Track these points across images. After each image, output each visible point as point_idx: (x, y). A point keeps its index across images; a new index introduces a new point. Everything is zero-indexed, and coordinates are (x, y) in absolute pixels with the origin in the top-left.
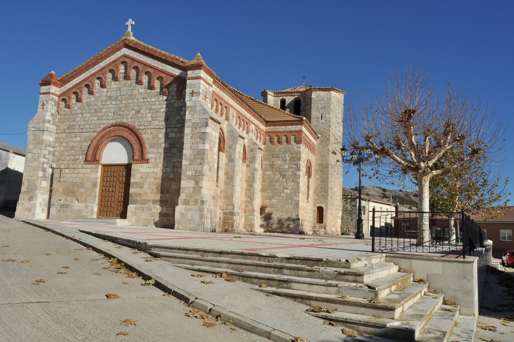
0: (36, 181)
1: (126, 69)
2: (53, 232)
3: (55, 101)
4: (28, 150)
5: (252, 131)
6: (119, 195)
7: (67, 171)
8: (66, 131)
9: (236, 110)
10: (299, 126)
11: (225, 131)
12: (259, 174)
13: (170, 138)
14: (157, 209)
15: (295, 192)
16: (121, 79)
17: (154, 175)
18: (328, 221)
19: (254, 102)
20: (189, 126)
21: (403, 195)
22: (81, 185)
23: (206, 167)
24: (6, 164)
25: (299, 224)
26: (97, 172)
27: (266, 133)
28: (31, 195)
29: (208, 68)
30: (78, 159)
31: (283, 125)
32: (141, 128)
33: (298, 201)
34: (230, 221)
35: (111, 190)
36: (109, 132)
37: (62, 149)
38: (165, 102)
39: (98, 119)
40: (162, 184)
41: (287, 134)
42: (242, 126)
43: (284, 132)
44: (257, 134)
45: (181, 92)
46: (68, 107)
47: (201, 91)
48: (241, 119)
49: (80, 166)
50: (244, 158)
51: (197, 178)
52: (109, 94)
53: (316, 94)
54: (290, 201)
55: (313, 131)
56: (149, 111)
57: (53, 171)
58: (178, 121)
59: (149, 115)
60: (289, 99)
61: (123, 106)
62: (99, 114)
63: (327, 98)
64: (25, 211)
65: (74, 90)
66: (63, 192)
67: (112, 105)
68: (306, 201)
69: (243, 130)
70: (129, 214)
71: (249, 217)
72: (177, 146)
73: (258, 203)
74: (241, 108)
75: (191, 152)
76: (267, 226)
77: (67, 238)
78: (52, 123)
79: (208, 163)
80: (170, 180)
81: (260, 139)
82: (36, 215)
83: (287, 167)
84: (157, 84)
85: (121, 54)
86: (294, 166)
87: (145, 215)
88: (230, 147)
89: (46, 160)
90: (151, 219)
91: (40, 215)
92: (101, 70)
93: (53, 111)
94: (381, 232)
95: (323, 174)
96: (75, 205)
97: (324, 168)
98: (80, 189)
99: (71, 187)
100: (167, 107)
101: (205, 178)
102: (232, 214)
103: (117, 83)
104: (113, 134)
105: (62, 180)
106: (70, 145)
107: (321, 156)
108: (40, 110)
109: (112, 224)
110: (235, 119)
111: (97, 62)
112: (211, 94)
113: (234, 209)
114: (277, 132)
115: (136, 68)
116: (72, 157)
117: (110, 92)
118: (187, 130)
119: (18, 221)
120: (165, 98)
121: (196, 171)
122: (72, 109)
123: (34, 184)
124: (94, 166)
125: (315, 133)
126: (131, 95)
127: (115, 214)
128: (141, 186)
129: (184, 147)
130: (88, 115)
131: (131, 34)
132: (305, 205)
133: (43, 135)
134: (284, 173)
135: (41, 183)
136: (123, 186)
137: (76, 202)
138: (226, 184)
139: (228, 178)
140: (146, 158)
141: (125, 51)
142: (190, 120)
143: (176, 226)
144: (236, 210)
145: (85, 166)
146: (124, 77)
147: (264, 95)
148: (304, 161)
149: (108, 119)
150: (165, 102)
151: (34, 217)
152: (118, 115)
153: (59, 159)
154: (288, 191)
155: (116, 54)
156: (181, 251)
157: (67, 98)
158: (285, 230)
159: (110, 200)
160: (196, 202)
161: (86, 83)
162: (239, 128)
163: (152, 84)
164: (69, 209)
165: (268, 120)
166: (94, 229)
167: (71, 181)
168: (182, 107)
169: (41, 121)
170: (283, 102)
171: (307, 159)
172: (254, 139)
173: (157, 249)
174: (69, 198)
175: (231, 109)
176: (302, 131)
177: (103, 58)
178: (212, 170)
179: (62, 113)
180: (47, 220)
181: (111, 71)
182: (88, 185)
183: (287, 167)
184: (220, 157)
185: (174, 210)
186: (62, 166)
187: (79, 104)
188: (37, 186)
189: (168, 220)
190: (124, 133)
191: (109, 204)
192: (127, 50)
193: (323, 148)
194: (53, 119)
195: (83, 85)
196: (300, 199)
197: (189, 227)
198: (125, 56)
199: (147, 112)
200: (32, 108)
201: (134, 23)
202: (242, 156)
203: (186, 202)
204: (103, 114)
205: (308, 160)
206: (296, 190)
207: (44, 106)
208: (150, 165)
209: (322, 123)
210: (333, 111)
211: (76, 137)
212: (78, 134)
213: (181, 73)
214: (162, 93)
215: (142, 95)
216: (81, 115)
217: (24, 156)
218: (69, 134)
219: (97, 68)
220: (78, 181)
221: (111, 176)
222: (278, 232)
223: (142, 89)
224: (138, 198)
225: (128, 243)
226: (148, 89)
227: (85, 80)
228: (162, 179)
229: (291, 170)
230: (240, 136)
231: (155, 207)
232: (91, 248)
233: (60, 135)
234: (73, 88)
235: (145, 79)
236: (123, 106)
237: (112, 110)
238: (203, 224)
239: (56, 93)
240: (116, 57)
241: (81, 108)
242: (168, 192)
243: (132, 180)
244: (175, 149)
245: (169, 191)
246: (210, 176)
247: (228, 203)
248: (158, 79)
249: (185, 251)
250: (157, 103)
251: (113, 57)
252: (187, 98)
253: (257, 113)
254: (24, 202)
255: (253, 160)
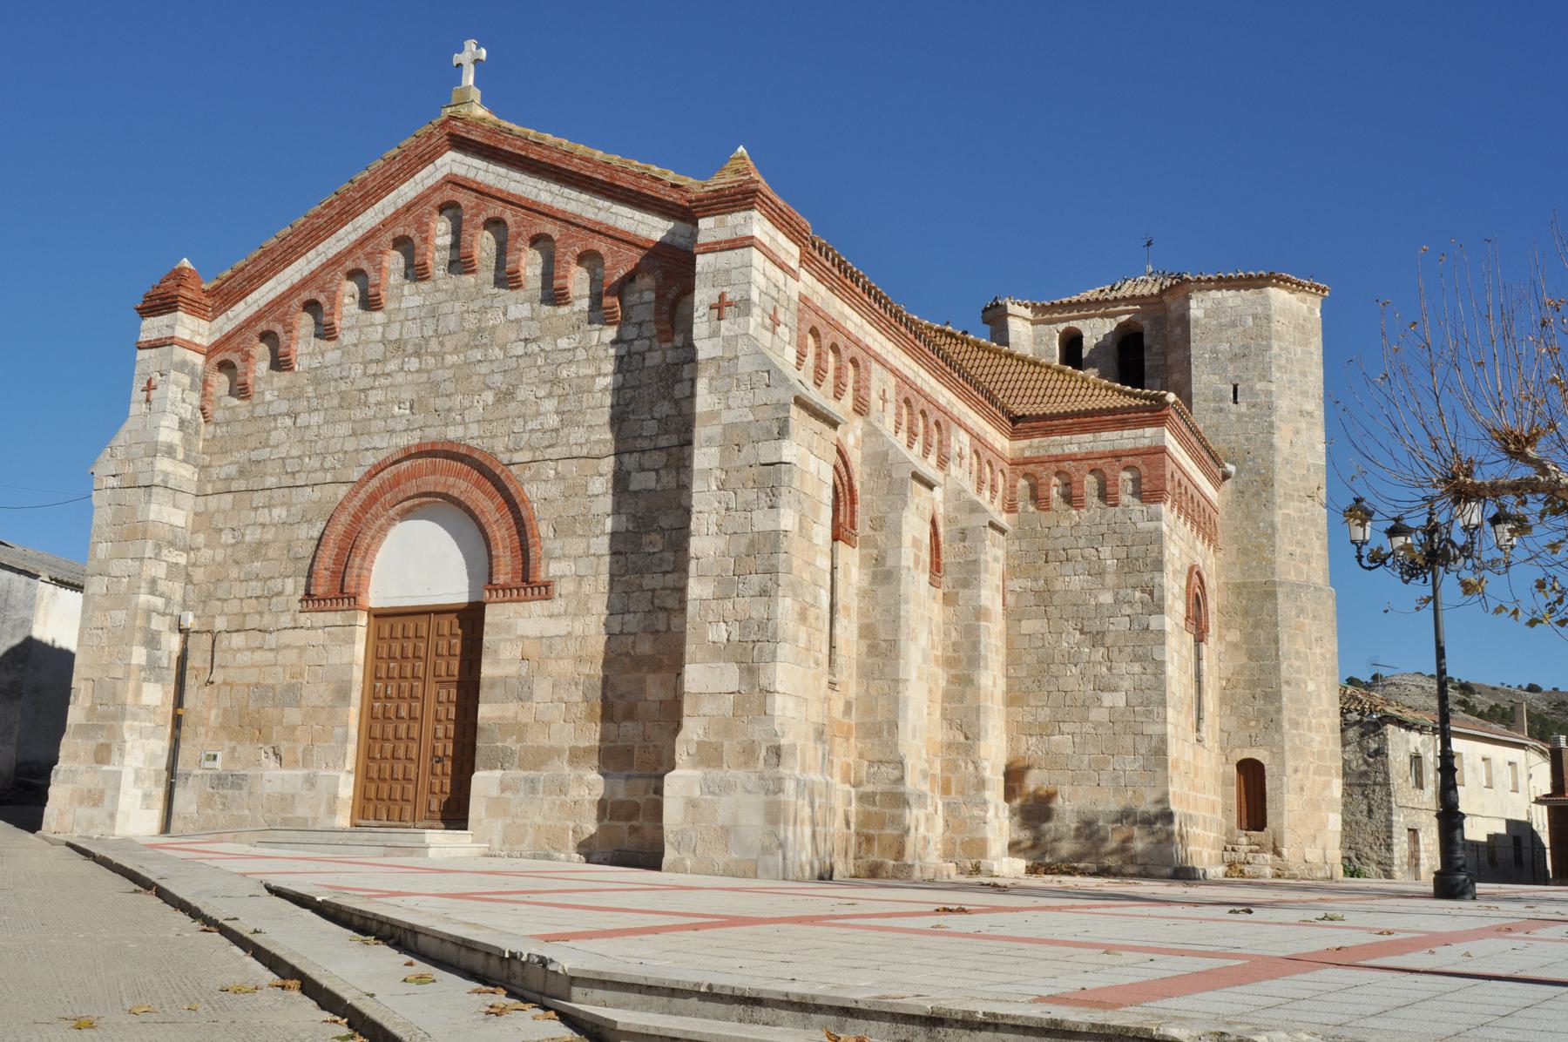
0: (120, 683)
1: (457, 232)
2: (162, 893)
3: (192, 373)
4: (91, 566)
5: (961, 456)
6: (439, 734)
7: (238, 640)
8: (234, 486)
9: (894, 372)
10: (1149, 431)
11: (855, 457)
12: (994, 635)
13: (636, 493)
14: (590, 786)
15: (1146, 703)
16: (439, 271)
17: (573, 646)
18: (1288, 819)
19: (960, 343)
20: (709, 441)
21: (1543, 707)
22: (292, 694)
23: (786, 606)
24: (27, 622)
25: (1170, 835)
26: (351, 641)
27: (1014, 463)
28: (101, 741)
29: (780, 203)
30: (279, 594)
31: (1084, 431)
32: (517, 457)
33: (1163, 739)
34: (888, 831)
35: (404, 713)
36: (396, 481)
37: (220, 554)
38: (612, 351)
39: (354, 434)
40: (605, 680)
41: (1100, 466)
42: (920, 438)
43: (1088, 457)
44: (980, 471)
45: (674, 304)
46: (241, 390)
47: (755, 296)
48: (917, 409)
49: (285, 620)
50: (936, 567)
51: (752, 651)
52: (394, 334)
53: (1209, 304)
54: (1128, 741)
55: (1207, 448)
56: (549, 388)
57: (185, 642)
58: (664, 423)
59: (549, 405)
60: (1095, 331)
61: (448, 374)
62: (358, 414)
63: (1255, 317)
64: (81, 803)
65: (262, 326)
66: (223, 727)
67: (405, 374)
68: (1193, 737)
69: (926, 453)
70: (477, 808)
71: (965, 812)
72: (665, 522)
73: (994, 753)
74: (915, 366)
75: (721, 543)
76: (1033, 847)
77: (210, 923)
78: (180, 456)
79: (795, 588)
80: (638, 663)
81: (993, 488)
82: (119, 818)
83: (1107, 598)
84: (578, 281)
85: (439, 176)
86: (1138, 594)
87: (540, 813)
88: (878, 524)
89: (159, 602)
90: (565, 830)
91: (135, 820)
92: (361, 243)
93: (187, 411)
94: (1492, 861)
95: (1256, 625)
96: (268, 774)
97: (1258, 600)
98: (287, 710)
99: (252, 706)
100: (619, 370)
101: (784, 650)
102: (899, 800)
103: (424, 286)
104: (411, 487)
105: (218, 676)
106: (248, 538)
107: (1244, 552)
108: (137, 408)
109: (410, 850)
110: (891, 408)
111: (346, 214)
112: (793, 307)
113: (902, 779)
114: (1057, 459)
115: (495, 224)
116: (256, 587)
117: (397, 326)
118: (704, 457)
119: (53, 843)
120: (611, 333)
121: (744, 623)
122: (256, 399)
123: (114, 696)
124: (337, 618)
125: (1214, 457)
126: (479, 330)
127: (422, 809)
128: (521, 691)
129: (693, 526)
130: (316, 419)
131: (476, 94)
132: (1189, 756)
133: (149, 502)
134: (1096, 625)
135: (138, 691)
136: (453, 696)
137: (272, 762)
138: (866, 674)
139: (873, 649)
140: (542, 576)
141: (453, 163)
142: (713, 415)
143: (669, 855)
144: (913, 783)
145: (304, 619)
146: (451, 263)
147: (996, 318)
148: (1175, 572)
149: (392, 432)
150: (612, 351)
151: (113, 826)
152: (427, 412)
153: (210, 596)
154: (1119, 700)
155: (418, 177)
156: (722, 1008)
157: (235, 358)
158: (1112, 862)
159: (401, 753)
160: (749, 752)
161: (306, 295)
162: (910, 446)
163: (556, 283)
164: (244, 793)
165: (1019, 410)
166: (319, 879)
167: (253, 680)
168: (679, 365)
169: (139, 450)
170: (1071, 346)
171: (1188, 564)
172: (969, 486)
173: (599, 994)
174: (245, 750)
175: (875, 366)
176: (1163, 450)
177: (370, 196)
178: (811, 619)
179: (219, 415)
180: (164, 840)
181: (402, 243)
182: (317, 694)
183: (1107, 598)
184: (840, 563)
185: (659, 791)
186: (220, 624)
187: (282, 379)
188: (124, 705)
189: (634, 830)
190: (451, 480)
191: (399, 768)
192: (458, 156)
193: (1247, 517)
194: (187, 441)
195: (296, 303)
196: (1170, 729)
197: (721, 859)
198: (453, 181)
199: (541, 393)
200: (106, 400)
201: (483, 53)
202: (925, 556)
203: (709, 756)
204: (370, 413)
205: (1191, 569)
206: (1153, 694)
207: (154, 394)
208: (557, 605)
209: (1240, 416)
210: (1280, 368)
211: (269, 507)
212: (276, 493)
213: (671, 233)
214: (598, 313)
215: (520, 330)
216: (288, 422)
217: (78, 588)
218: (246, 496)
219: (348, 235)
220: (280, 678)
221: (404, 657)
222: (1083, 873)
223: (520, 306)
224: (511, 743)
225: (464, 957)
226: (543, 301)
227: (304, 283)
228: (607, 664)
229: (1127, 610)
230: (916, 476)
231: (580, 779)
232: (295, 983)
233: (213, 503)
234: (259, 316)
235: (530, 265)
236: (448, 374)
237: (407, 395)
238: (781, 845)
239: (198, 340)
240: (420, 189)
241: (288, 393)
242: (630, 715)
243: (487, 670)
244: (655, 537)
245: (638, 709)
246: (802, 643)
247: (878, 756)
248: (581, 259)
249: (739, 1009)
250: (581, 354)
251: (408, 191)
252: (700, 328)
253: (977, 386)
254: (75, 766)
255: (970, 574)
